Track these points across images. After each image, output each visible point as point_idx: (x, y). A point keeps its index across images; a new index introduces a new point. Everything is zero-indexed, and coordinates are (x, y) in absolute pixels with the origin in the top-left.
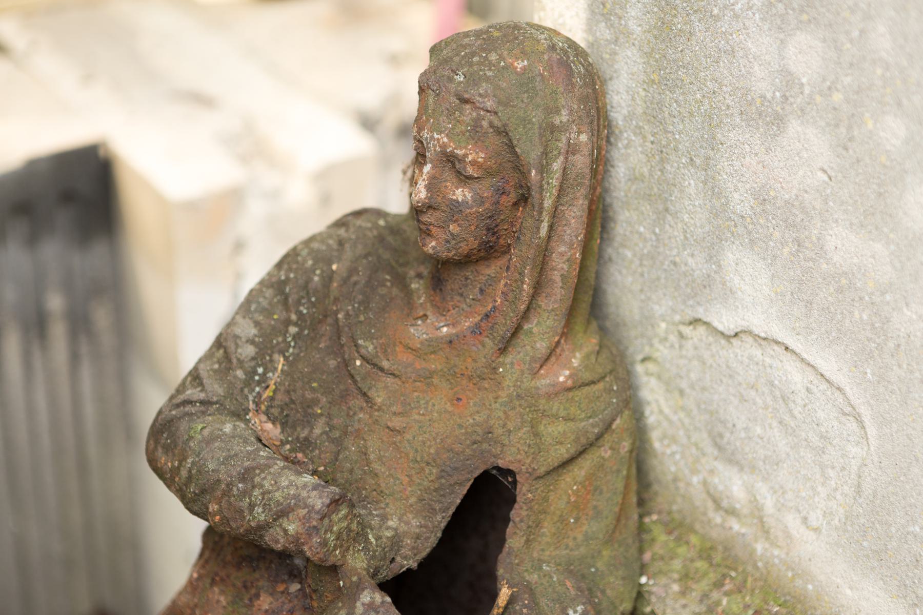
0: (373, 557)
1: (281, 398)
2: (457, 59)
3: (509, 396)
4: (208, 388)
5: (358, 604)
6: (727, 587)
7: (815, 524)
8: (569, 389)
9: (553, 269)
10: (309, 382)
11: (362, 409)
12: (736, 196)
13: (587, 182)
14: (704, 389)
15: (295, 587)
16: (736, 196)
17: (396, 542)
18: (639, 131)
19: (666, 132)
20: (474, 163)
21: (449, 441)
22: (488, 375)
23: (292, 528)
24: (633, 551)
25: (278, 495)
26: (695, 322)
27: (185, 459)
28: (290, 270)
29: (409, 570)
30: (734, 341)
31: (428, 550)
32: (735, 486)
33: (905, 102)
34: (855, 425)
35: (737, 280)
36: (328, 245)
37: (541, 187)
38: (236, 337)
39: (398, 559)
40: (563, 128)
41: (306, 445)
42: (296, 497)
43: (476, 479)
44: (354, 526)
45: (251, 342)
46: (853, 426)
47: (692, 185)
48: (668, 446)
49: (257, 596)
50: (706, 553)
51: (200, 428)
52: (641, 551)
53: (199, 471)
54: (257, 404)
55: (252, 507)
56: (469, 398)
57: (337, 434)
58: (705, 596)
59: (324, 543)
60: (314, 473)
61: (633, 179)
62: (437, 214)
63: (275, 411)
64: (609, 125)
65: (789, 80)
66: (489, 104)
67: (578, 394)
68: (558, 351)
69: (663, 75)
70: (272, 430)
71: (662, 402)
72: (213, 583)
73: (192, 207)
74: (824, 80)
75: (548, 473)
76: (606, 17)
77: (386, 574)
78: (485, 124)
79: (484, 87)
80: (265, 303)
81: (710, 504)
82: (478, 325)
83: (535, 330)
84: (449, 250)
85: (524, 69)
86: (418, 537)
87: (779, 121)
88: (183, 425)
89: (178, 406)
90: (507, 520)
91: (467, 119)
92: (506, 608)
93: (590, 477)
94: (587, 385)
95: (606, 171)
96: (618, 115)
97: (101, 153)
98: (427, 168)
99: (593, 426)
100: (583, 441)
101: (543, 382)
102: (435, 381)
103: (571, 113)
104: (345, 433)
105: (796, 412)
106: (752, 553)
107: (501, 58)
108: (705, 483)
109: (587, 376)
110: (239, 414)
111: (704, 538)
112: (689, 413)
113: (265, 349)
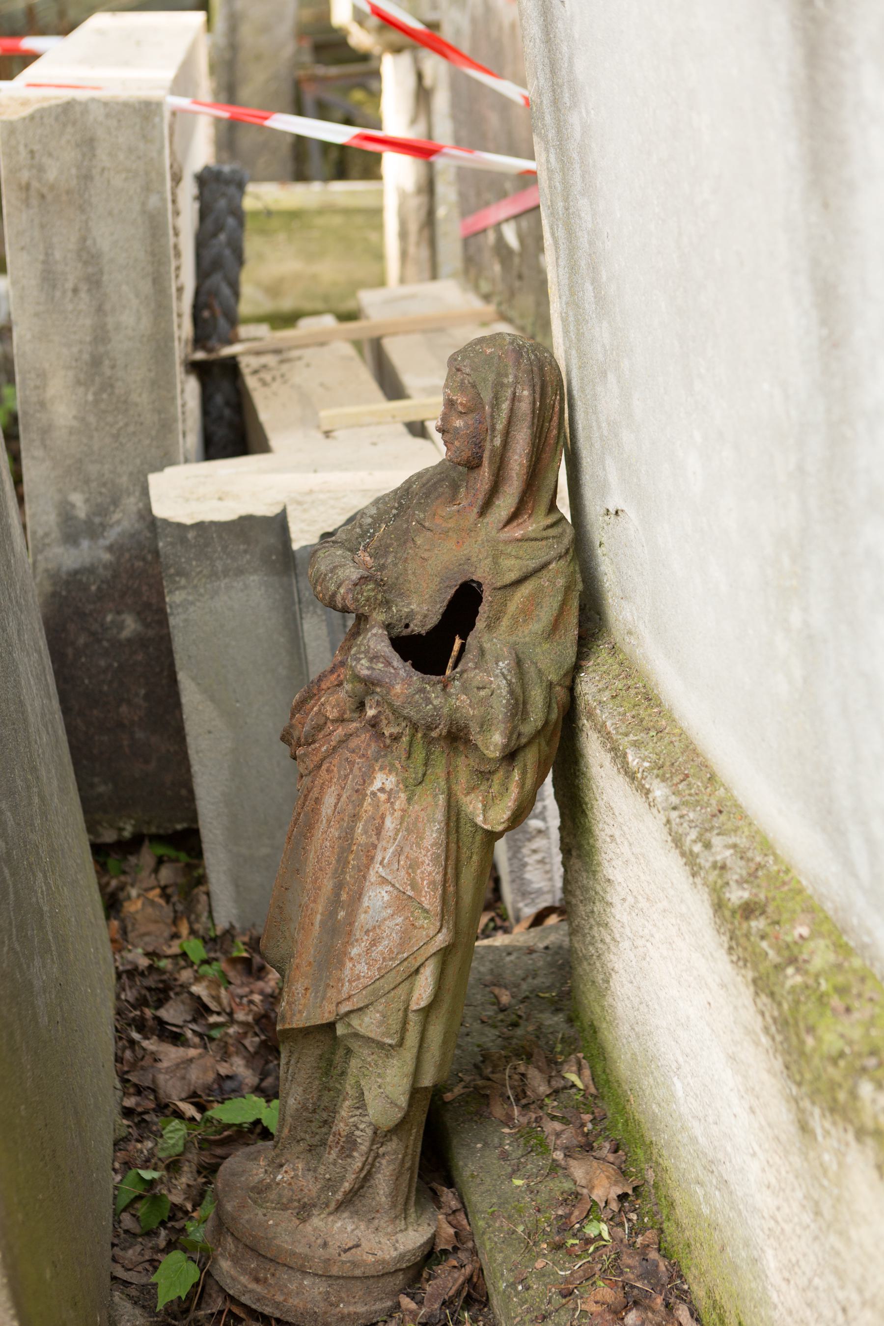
17: (411, 615)
20: (461, 404)
39: (412, 625)
45: (371, 517)
66: (468, 370)
75: (505, 587)
77: (399, 630)
78: (466, 381)
85: (491, 353)
91: (458, 379)
94: (532, 540)
102: (450, 534)
107: (482, 348)
113: (377, 520)
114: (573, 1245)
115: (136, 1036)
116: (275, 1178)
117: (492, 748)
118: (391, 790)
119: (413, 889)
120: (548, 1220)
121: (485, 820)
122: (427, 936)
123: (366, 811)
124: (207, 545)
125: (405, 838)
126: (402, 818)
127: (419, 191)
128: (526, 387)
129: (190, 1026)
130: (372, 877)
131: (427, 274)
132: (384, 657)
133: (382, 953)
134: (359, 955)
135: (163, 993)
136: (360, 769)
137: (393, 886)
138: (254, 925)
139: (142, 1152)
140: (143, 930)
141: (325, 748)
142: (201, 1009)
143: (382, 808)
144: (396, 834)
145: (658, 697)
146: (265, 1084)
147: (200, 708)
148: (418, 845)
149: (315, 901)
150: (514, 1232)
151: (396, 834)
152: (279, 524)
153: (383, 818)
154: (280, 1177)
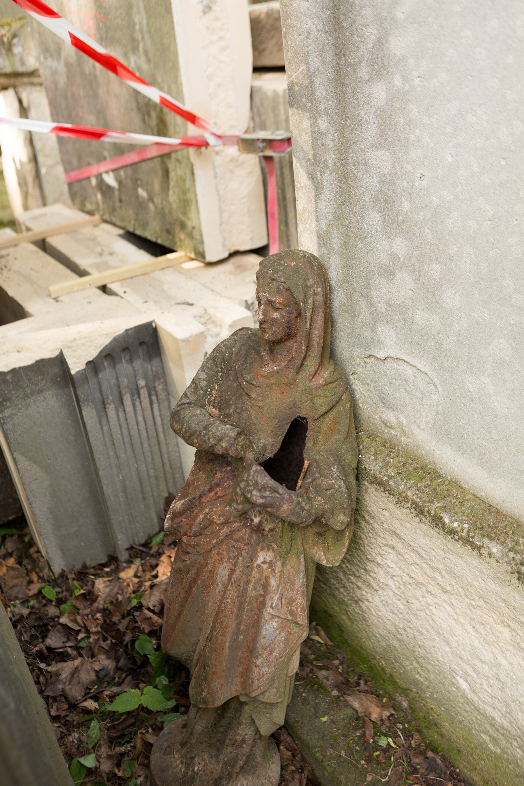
0: (256, 454)
1: (218, 399)
3: (302, 390)
4: (190, 398)
7: (422, 427)
8: (324, 385)
15: (229, 468)
17: (264, 448)
18: (341, 287)
20: (279, 303)
22: (293, 383)
23: (224, 445)
24: (355, 445)
25: (218, 434)
27: (183, 424)
29: (270, 458)
32: (391, 417)
33: (439, 257)
35: (383, 338)
37: (305, 309)
38: (199, 379)
40: (312, 286)
41: (228, 416)
42: (224, 433)
44: (247, 443)
45: (205, 380)
46: (433, 387)
47: (363, 304)
48: (365, 405)
49: (216, 473)
50: (383, 444)
51: (188, 413)
52: (358, 445)
55: (209, 439)
57: (239, 410)
58: (384, 459)
59: (236, 449)
62: (268, 324)
63: (216, 404)
64: (330, 285)
65: (395, 257)
66: (282, 280)
69: (348, 264)
72: (200, 471)
75: (319, 417)
77: (262, 460)
78: (281, 287)
80: (209, 366)
81: (383, 425)
82: (287, 365)
85: (294, 265)
86: (272, 445)
87: (392, 273)
88: (182, 413)
89: (180, 406)
90: (305, 436)
91: (275, 286)
92: (308, 469)
93: (335, 418)
95: (331, 304)
98: (262, 307)
100: (331, 404)
101: (314, 384)
104: (242, 410)
107: (286, 262)
108: (380, 417)
109: (330, 380)
110: (203, 407)
112: (371, 392)
113: (210, 382)
114: (378, 756)
115: (42, 665)
116: (194, 769)
117: (339, 524)
118: (271, 561)
119: (291, 615)
120: (353, 740)
122: (298, 636)
124: (19, 381)
125: (283, 588)
126: (280, 577)
127: (30, 161)
129: (67, 644)
130: (266, 615)
131: (40, 202)
132: (271, 488)
133: (275, 657)
134: (263, 663)
135: (44, 628)
137: (279, 617)
138: (74, 566)
139: (73, 742)
140: (11, 584)
141: (215, 541)
142: (68, 631)
144: (278, 587)
145: (435, 471)
146: (120, 664)
147: (29, 468)
148: (292, 589)
149: (223, 635)
150: (340, 756)
151: (278, 587)
152: (60, 361)
153: (267, 579)
154: (196, 768)
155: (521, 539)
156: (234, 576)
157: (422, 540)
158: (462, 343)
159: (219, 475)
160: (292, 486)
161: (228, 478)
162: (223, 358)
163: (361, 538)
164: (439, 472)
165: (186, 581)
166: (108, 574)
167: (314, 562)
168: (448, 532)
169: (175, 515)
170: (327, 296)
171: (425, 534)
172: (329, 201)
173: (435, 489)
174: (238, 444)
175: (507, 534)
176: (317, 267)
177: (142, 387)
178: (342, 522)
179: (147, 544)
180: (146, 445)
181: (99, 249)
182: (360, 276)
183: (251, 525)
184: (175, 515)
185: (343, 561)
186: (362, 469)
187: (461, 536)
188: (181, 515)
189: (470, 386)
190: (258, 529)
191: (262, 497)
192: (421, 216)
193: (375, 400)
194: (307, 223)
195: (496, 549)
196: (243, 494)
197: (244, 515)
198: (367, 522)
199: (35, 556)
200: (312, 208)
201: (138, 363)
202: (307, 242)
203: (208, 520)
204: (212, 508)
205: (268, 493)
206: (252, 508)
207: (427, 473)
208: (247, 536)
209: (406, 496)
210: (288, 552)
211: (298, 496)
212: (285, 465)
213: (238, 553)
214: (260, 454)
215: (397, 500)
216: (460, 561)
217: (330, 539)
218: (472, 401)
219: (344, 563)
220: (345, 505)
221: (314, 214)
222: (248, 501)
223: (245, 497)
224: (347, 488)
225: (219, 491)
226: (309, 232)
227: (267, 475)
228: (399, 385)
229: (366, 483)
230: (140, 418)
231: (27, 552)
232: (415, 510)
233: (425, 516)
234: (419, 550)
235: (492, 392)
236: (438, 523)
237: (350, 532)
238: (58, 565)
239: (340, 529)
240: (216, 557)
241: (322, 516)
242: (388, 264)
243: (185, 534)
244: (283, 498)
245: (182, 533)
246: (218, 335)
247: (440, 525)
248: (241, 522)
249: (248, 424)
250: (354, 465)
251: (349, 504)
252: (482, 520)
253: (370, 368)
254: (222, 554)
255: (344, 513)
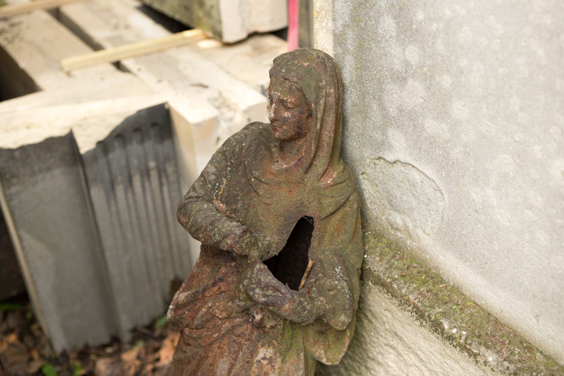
0: (261, 251)
2: (282, 63)
4: (198, 192)
5: (255, 269)
6: (397, 258)
7: (428, 232)
8: (332, 186)
9: (324, 141)
10: (235, 188)
11: (255, 197)
12: (391, 109)
13: (334, 107)
14: (384, 183)
15: (233, 264)
16: (391, 109)
17: (269, 245)
19: (364, 87)
20: (290, 102)
21: (288, 207)
22: (301, 182)
23: (229, 242)
24: (361, 245)
26: (380, 158)
27: (190, 218)
28: (227, 146)
30: (394, 164)
31: (282, 248)
32: (398, 219)
33: (450, 69)
34: (440, 194)
36: (241, 137)
37: (316, 110)
38: (208, 172)
39: (271, 252)
40: (324, 87)
41: (235, 211)
42: (230, 230)
43: (299, 221)
44: (253, 240)
45: (214, 174)
46: (439, 194)
47: (375, 106)
48: (373, 205)
49: (220, 268)
50: (389, 245)
51: (195, 207)
52: (364, 245)
53: (195, 223)
54: (217, 197)
55: (215, 235)
56: (294, 191)
58: (389, 261)
59: (241, 247)
60: (239, 221)
61: (354, 105)
62: (279, 122)
63: (223, 199)
64: (343, 85)
65: (407, 64)
66: (295, 80)
67: (336, 187)
68: (327, 171)
69: (362, 65)
70: (222, 206)
71: (370, 189)
73: (198, 125)
74: (420, 63)
75: (326, 217)
76: (340, 44)
77: (266, 257)
78: (294, 87)
79: (293, 73)
80: (218, 159)
81: (389, 227)
82: (296, 164)
83: (318, 164)
84: (284, 136)
85: (308, 66)
86: (278, 243)
87: (405, 80)
88: (189, 206)
89: (187, 199)
90: (310, 236)
91: (287, 86)
92: (311, 268)
93: (342, 218)
96: (347, 82)
97: (166, 107)
98: (274, 105)
99: (342, 199)
100: (338, 205)
101: (322, 184)
103: (326, 81)
104: (249, 206)
105: (418, 190)
106: (406, 244)
107: (299, 62)
109: (339, 181)
110: (210, 201)
111: (388, 240)
112: (380, 193)
113: (219, 176)
117: (340, 324)
118: (271, 357)
121: (328, 360)
123: (254, 372)
128: (332, 87)
132: (273, 287)
136: (248, 348)
141: (217, 335)
143: (265, 369)
155: (517, 349)
156: (234, 370)
157: (422, 343)
158: (469, 154)
159: (223, 270)
160: (294, 286)
161: (232, 273)
162: (233, 152)
163: (363, 336)
164: (442, 278)
165: (187, 373)
166: (110, 355)
167: (314, 359)
168: (446, 338)
169: (178, 307)
170: (339, 96)
171: (425, 338)
172: (345, 2)
173: (436, 294)
174: (243, 242)
175: (503, 343)
176: (331, 68)
177: (153, 169)
178: (343, 323)
179: (151, 327)
180: (154, 227)
181: (114, 21)
182: (373, 79)
183: (252, 321)
184: (178, 307)
185: (344, 357)
186: (367, 270)
187: (459, 342)
188: (184, 307)
189: (475, 197)
190: (260, 326)
191: (264, 296)
192: (434, 27)
193: (383, 202)
194: (323, 22)
195: (491, 358)
196: (246, 291)
197: (246, 311)
198: (370, 321)
199: (37, 333)
200: (329, 7)
201: (149, 145)
202: (323, 42)
203: (211, 313)
204: (215, 303)
205: (270, 292)
206: (255, 305)
207: (429, 277)
208: (248, 332)
209: (408, 300)
210: (288, 350)
211: (300, 296)
212: (289, 263)
213: (239, 348)
214: (265, 252)
215: (399, 302)
216: (457, 367)
217: (331, 338)
218: (476, 211)
219: (346, 358)
220: (347, 307)
221: (330, 13)
222: (250, 298)
223: (248, 295)
224: (349, 290)
225: (223, 286)
226: (325, 30)
227: (271, 273)
228: (407, 189)
229: (370, 283)
230: (149, 200)
231: (28, 328)
232: (416, 313)
233: (425, 320)
234: (419, 352)
235: (495, 204)
236: (438, 328)
237: (351, 331)
238: (60, 343)
239: (341, 329)
240: (217, 350)
241: (324, 316)
242: (400, 70)
243: (187, 326)
244: (285, 298)
245: (184, 325)
246: (231, 120)
247: (439, 331)
248: (243, 318)
249: (255, 221)
250: (359, 266)
251: (351, 306)
252: (480, 327)
253: (379, 170)
254: (223, 348)
255: (345, 313)
